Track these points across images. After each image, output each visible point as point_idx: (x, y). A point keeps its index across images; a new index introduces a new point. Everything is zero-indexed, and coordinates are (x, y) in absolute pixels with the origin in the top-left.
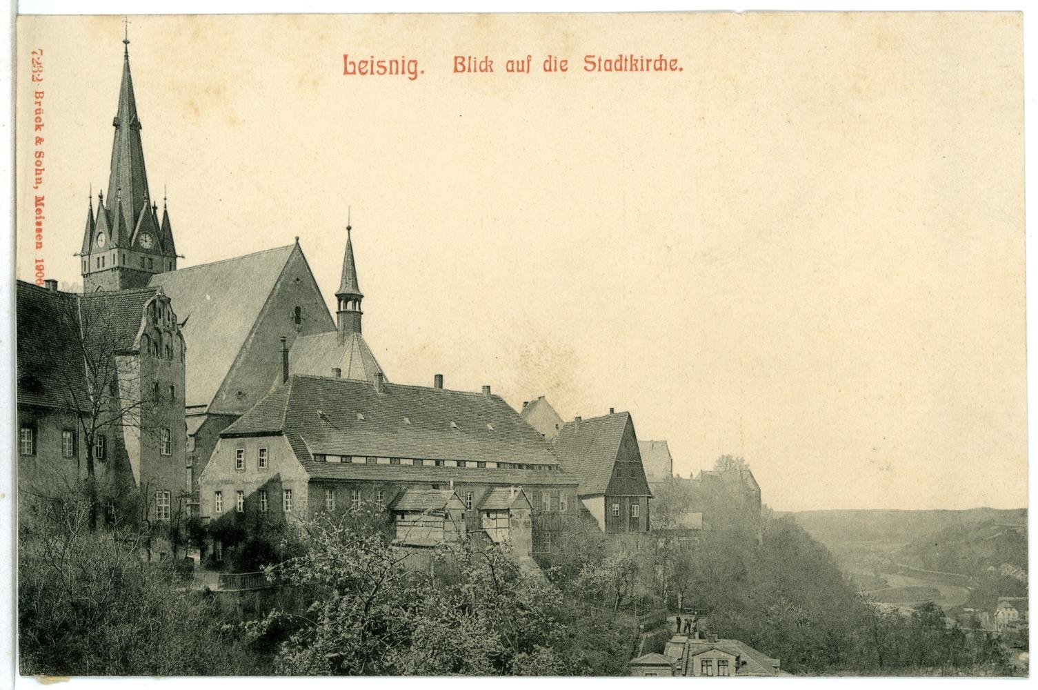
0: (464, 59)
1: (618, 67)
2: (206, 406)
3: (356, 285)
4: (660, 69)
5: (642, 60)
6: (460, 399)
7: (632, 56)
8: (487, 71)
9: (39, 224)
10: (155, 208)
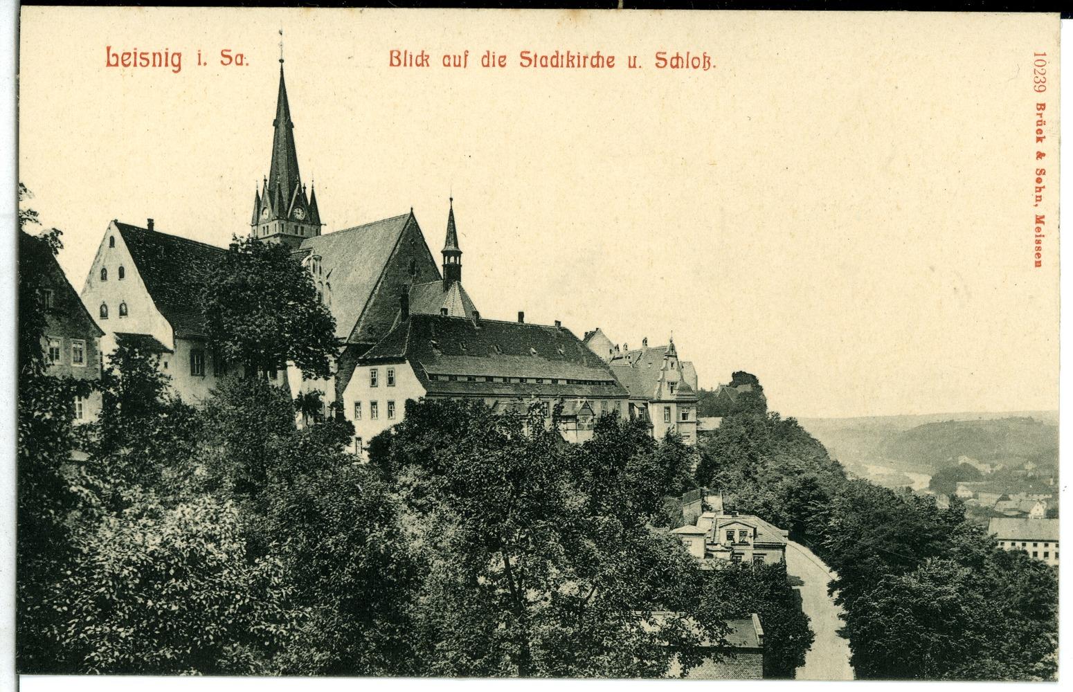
0: (399, 53)
1: (555, 63)
2: (345, 338)
3: (456, 244)
4: (598, 65)
5: (579, 57)
6: (537, 330)
7: (568, 53)
8: (423, 65)
9: (1038, 242)
10: (305, 188)
